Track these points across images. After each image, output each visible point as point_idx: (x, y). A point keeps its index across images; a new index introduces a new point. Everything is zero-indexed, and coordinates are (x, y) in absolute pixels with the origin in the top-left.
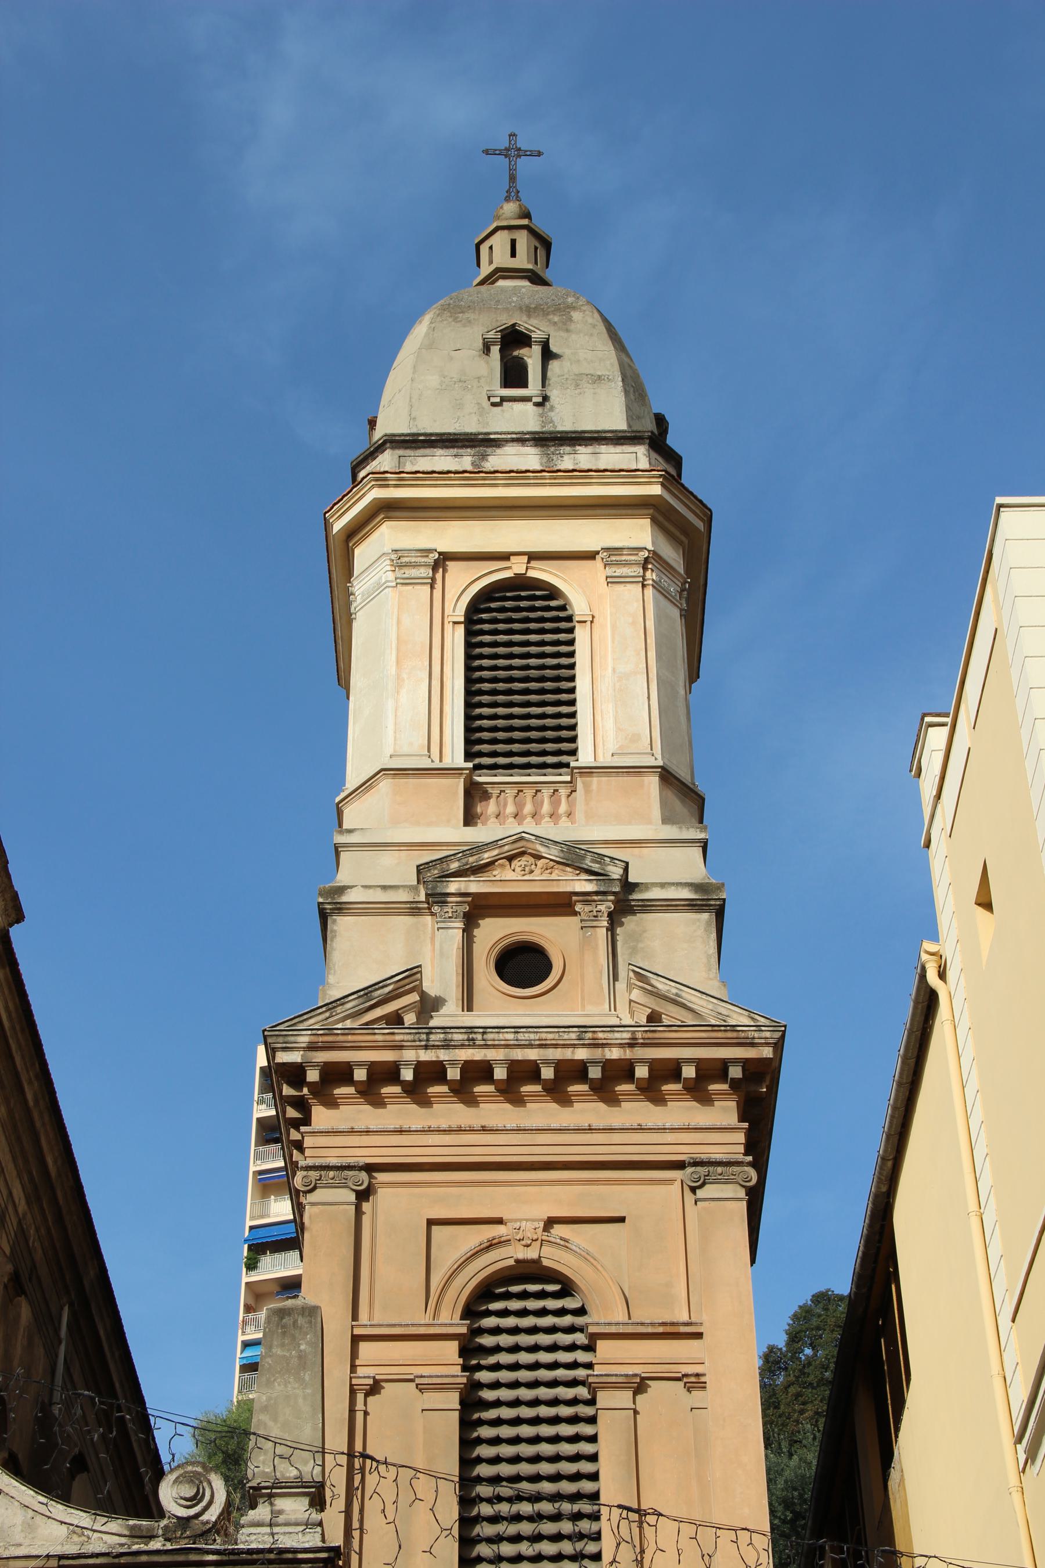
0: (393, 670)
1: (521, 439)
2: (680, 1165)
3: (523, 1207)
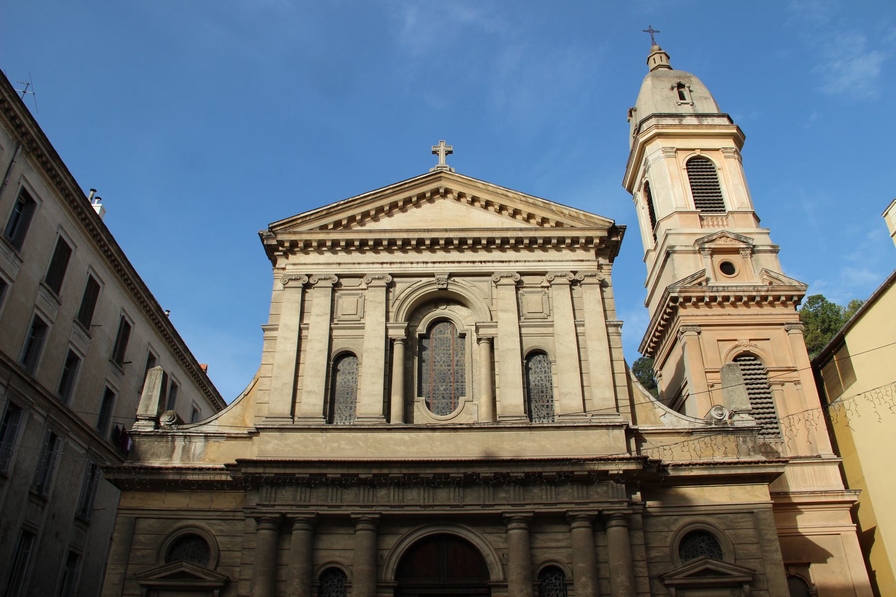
0: (670, 182)
1: (691, 116)
2: (782, 324)
3: (744, 337)
